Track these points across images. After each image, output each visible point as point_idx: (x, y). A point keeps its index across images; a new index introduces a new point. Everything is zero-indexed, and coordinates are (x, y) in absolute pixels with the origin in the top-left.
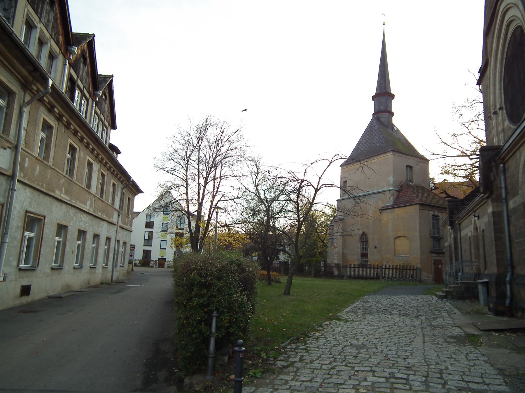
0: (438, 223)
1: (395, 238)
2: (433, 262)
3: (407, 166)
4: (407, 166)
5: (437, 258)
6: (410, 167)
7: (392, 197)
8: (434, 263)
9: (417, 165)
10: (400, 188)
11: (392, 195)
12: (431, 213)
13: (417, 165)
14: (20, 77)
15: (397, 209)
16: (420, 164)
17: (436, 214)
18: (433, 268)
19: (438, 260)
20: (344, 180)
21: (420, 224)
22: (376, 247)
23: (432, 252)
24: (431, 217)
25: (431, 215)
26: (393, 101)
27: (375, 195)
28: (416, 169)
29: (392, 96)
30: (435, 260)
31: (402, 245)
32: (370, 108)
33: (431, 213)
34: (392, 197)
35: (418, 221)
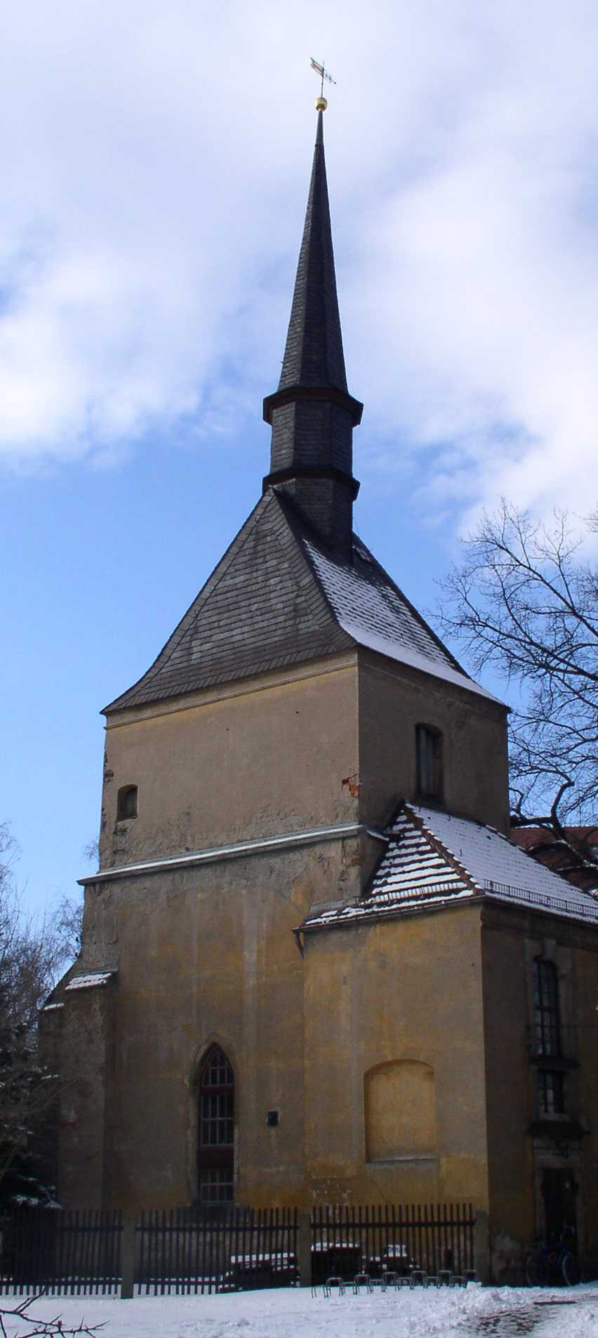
2: (538, 1182)
3: (418, 728)
20: (119, 783)
22: (273, 1119)
27: (276, 862)
30: (547, 1171)
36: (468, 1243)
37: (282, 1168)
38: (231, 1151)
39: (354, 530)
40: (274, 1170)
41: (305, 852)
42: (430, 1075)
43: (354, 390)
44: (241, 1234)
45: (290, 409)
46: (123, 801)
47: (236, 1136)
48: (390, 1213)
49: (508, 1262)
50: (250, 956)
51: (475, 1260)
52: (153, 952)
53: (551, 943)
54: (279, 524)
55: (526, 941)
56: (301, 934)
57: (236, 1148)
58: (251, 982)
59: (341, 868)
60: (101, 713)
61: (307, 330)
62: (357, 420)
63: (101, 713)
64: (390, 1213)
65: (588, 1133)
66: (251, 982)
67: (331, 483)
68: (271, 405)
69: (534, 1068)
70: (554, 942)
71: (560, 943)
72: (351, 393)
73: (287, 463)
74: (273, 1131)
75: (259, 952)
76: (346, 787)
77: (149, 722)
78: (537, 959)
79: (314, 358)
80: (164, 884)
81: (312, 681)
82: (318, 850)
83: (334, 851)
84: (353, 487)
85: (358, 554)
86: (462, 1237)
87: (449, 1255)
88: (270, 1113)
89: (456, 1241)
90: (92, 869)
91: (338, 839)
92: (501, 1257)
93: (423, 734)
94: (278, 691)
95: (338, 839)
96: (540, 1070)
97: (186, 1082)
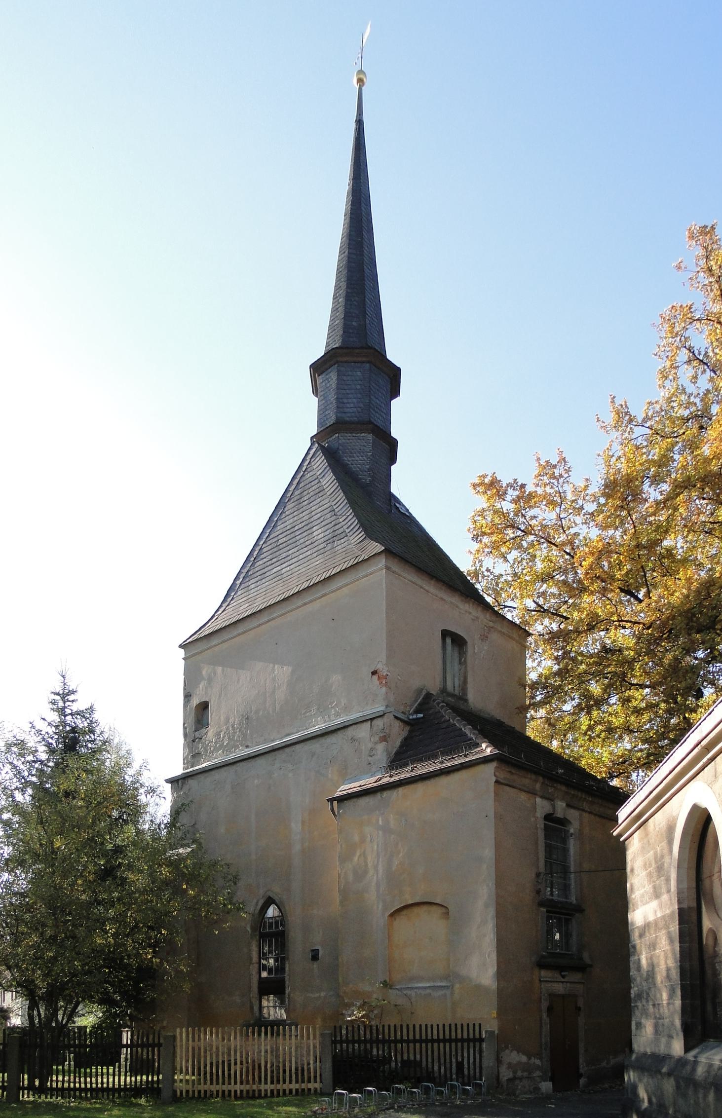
0: (565, 851)
1: (392, 915)
2: (545, 1005)
3: (445, 634)
4: (445, 634)
5: (559, 988)
6: (454, 640)
7: (381, 747)
8: (550, 1010)
9: (484, 638)
10: (417, 712)
11: (384, 739)
12: (542, 807)
13: (484, 638)
14: (293, 1054)
15: (401, 790)
16: (494, 636)
17: (559, 814)
18: (546, 1029)
19: (563, 997)
20: (195, 701)
21: (498, 846)
22: (315, 956)
23: (542, 965)
24: (541, 824)
25: (540, 814)
26: (394, 403)
27: (315, 746)
28: (478, 650)
29: (394, 374)
30: (552, 996)
31: (419, 944)
32: (299, 417)
33: (542, 807)
34: (381, 747)
35: (488, 835)
36: (477, 1056)
37: (323, 994)
38: (284, 981)
39: (394, 490)
40: (317, 995)
41: (340, 734)
42: (446, 914)
43: (392, 355)
44: (411, 1037)
45: (333, 375)
46: (198, 716)
47: (287, 969)
48: (459, 1031)
49: (515, 1072)
50: (296, 827)
51: (484, 1072)
52: (222, 830)
53: (561, 805)
54: (320, 462)
55: (538, 800)
56: (335, 803)
57: (287, 979)
58: (297, 848)
59: (370, 745)
60: (180, 646)
61: (348, 298)
62: (395, 392)
63: (180, 646)
64: (459, 1031)
65: (591, 966)
66: (297, 848)
67: (370, 437)
68: (318, 368)
69: (544, 910)
70: (564, 805)
71: (568, 805)
72: (389, 356)
73: (332, 420)
74: (315, 965)
75: (303, 822)
76: (375, 677)
77: (216, 649)
78: (548, 817)
79: (354, 323)
80: (229, 772)
81: (345, 590)
82: (350, 732)
83: (363, 732)
84: (393, 445)
85: (397, 508)
86: (471, 1051)
87: (460, 1065)
88: (313, 951)
89: (466, 1055)
90: (178, 770)
91: (366, 721)
92: (508, 1068)
93: (449, 641)
94: (316, 605)
95: (366, 721)
96: (548, 911)
97: (249, 929)
